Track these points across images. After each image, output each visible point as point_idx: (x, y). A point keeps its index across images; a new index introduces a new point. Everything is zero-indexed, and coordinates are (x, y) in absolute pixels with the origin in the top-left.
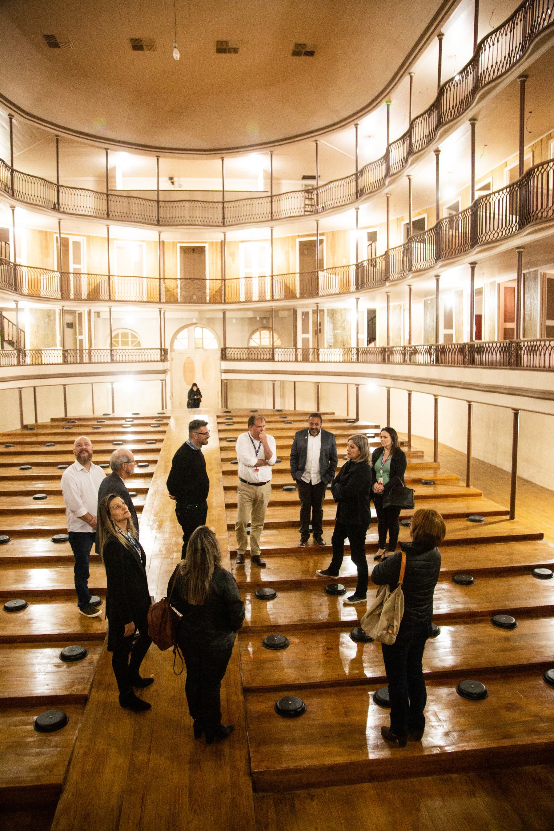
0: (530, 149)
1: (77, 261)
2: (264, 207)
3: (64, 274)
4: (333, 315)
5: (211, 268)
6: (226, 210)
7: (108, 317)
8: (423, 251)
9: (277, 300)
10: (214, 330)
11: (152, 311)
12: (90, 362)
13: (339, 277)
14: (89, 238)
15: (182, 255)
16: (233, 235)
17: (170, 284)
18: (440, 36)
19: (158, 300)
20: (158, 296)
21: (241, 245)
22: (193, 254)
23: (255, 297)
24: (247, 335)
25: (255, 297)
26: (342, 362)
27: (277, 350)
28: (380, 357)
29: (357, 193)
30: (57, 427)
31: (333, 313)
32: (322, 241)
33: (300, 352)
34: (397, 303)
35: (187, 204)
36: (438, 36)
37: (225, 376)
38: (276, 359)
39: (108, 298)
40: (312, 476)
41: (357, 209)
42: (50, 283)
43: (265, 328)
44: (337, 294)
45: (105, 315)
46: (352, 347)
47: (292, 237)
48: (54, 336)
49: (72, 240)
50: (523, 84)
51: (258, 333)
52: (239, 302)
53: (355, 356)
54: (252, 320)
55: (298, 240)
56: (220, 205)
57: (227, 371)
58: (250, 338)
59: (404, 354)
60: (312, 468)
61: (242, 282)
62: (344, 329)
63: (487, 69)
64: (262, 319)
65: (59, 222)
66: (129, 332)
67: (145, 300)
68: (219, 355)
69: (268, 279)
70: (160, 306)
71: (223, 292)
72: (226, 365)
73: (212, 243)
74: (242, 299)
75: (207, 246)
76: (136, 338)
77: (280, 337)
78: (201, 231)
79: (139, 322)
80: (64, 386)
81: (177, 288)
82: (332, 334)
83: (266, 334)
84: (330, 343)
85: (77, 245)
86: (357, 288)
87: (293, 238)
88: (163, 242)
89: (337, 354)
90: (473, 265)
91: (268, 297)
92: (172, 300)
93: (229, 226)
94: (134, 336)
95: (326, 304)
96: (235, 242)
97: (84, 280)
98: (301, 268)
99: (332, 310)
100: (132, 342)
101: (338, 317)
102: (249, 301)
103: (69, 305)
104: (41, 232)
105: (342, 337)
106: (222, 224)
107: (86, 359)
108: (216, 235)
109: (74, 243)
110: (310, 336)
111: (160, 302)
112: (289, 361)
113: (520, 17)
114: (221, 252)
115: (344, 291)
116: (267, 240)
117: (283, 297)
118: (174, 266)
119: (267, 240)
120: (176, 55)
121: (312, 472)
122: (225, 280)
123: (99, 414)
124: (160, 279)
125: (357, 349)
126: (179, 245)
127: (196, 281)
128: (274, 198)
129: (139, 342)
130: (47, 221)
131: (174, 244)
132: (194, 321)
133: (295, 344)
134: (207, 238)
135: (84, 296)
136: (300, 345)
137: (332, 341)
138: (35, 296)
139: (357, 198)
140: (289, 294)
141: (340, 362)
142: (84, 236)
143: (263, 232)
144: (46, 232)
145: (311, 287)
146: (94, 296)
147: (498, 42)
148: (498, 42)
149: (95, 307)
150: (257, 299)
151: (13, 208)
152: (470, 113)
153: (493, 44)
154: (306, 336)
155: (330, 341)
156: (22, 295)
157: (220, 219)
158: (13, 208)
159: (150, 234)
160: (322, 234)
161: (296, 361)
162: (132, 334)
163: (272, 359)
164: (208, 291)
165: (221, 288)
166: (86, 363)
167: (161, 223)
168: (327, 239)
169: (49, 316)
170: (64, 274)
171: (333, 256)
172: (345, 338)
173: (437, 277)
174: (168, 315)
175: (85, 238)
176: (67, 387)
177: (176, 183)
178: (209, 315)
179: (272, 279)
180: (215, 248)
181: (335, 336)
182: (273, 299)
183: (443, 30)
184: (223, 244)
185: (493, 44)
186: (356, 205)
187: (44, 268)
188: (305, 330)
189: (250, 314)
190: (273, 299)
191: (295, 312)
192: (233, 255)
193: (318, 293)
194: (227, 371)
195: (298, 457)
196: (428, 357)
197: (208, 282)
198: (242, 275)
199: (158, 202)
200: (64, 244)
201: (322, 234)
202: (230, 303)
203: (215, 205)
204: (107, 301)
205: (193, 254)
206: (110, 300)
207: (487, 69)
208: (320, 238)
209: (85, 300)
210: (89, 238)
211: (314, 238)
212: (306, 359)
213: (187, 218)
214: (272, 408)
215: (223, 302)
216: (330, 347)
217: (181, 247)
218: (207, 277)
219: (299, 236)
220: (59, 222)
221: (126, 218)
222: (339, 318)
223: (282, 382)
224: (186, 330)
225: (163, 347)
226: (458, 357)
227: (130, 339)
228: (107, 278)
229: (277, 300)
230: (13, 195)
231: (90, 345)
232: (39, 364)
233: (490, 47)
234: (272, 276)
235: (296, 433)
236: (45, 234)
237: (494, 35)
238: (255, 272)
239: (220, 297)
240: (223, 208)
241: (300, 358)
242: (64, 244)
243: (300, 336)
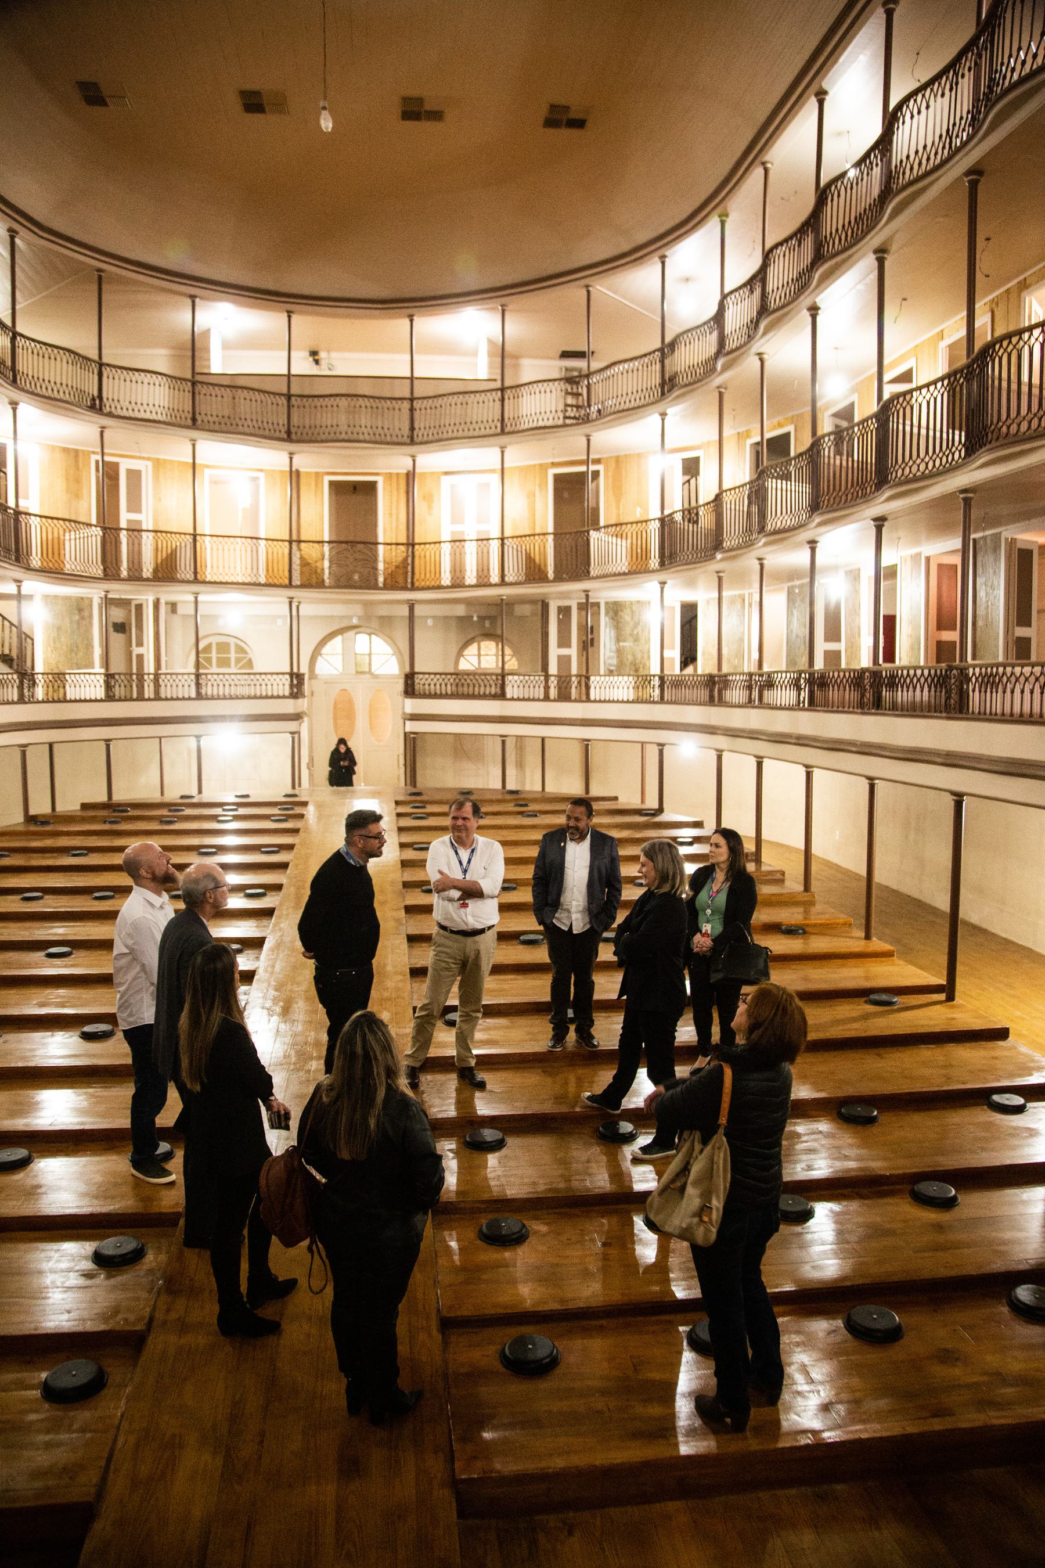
0: (987, 308)
1: (135, 505)
2: (487, 410)
3: (110, 531)
4: (616, 613)
5: (388, 524)
6: (417, 414)
7: (193, 612)
8: (787, 495)
9: (511, 584)
10: (392, 641)
11: (275, 604)
12: (157, 698)
13: (629, 541)
14: (158, 464)
15: (334, 496)
16: (429, 460)
17: (310, 551)
18: (821, 96)
19: (287, 582)
20: (287, 574)
21: (444, 479)
22: (354, 496)
23: (471, 578)
24: (454, 649)
25: (471, 578)
26: (633, 702)
27: (510, 677)
28: (704, 694)
29: (662, 385)
30: (93, 819)
31: (616, 609)
32: (596, 474)
33: (553, 682)
34: (737, 592)
35: (343, 402)
36: (816, 95)
37: (411, 726)
38: (509, 696)
39: (191, 577)
40: (574, 916)
41: (663, 415)
42: (82, 548)
43: (489, 636)
44: (624, 574)
45: (186, 609)
46: (652, 673)
47: (541, 465)
48: (89, 646)
49: (125, 465)
50: (974, 186)
51: (475, 645)
52: (440, 587)
53: (657, 692)
54: (463, 621)
55: (552, 472)
56: (406, 405)
57: (415, 717)
58: (460, 654)
59: (750, 688)
60: (574, 903)
61: (446, 549)
62: (636, 640)
63: (908, 157)
64: (482, 619)
65: (102, 433)
66: (232, 641)
67: (262, 580)
68: (400, 686)
69: (495, 545)
70: (291, 593)
71: (409, 568)
72: (412, 705)
73: (389, 476)
74: (446, 580)
75: (380, 480)
76: (246, 652)
77: (516, 653)
78: (372, 452)
79: (249, 622)
80: (108, 742)
81: (324, 559)
82: (614, 648)
83: (489, 647)
84: (611, 665)
85: (134, 476)
86: (662, 564)
87: (543, 468)
88: (298, 472)
89: (623, 687)
90: (880, 522)
91: (495, 578)
92: (312, 581)
93: (421, 443)
94: (240, 650)
95: (605, 593)
96: (433, 473)
97: (148, 542)
98: (555, 528)
99: (616, 603)
100: (238, 660)
101: (626, 616)
102: (458, 584)
103: (118, 590)
104: (65, 450)
105: (634, 655)
106: (408, 441)
107: (149, 691)
108: (398, 461)
109: (129, 472)
110: (573, 652)
111: (290, 585)
112: (534, 700)
113: (968, 62)
114: (407, 493)
115: (638, 569)
116: (493, 471)
117: (522, 578)
118: (318, 517)
119: (493, 471)
120: (327, 123)
121: (573, 910)
122: (413, 545)
123: (172, 795)
124: (290, 542)
125: (662, 678)
126: (327, 479)
127: (360, 546)
128: (508, 393)
129: (250, 661)
130: (77, 430)
131: (318, 476)
132: (355, 621)
133: (545, 668)
134: (383, 465)
135: (147, 571)
136: (553, 669)
137: (615, 662)
138: (54, 572)
139: (663, 394)
140: (534, 573)
141: (628, 702)
142: (149, 459)
143: (486, 456)
144: (76, 451)
145: (574, 561)
146: (166, 572)
147: (928, 107)
148: (928, 107)
149: (169, 593)
150: (474, 581)
151: (14, 405)
152: (875, 239)
153: (919, 112)
154: (564, 651)
155: (611, 661)
156: (28, 568)
157: (406, 431)
158: (14, 405)
159: (273, 457)
160: (598, 461)
161: (547, 698)
162: (237, 645)
163: (501, 696)
164: (381, 566)
165: (406, 559)
166: (149, 699)
167: (293, 437)
168: (606, 470)
169: (80, 610)
170: (110, 531)
171: (618, 501)
172: (639, 656)
173: (813, 544)
174: (306, 610)
175: (150, 464)
176: (112, 744)
177: (323, 363)
178: (383, 611)
179: (503, 545)
180: (394, 484)
181: (619, 652)
182: (503, 583)
183: (825, 85)
184: (410, 477)
185: (919, 112)
186: (660, 407)
187: (73, 518)
188: (564, 641)
189: (460, 610)
190: (503, 583)
191: (545, 606)
192: (429, 498)
193: (589, 572)
194: (415, 717)
195: (548, 879)
196: (794, 693)
197: (381, 549)
198: (446, 536)
199: (289, 397)
200: (109, 474)
201: (598, 461)
202: (423, 589)
203: (397, 405)
204: (188, 582)
205: (354, 496)
206: (196, 581)
207: (908, 157)
208: (593, 468)
209: (148, 580)
210: (158, 464)
211: (583, 469)
212: (564, 696)
213: (344, 428)
214: (500, 787)
215: (409, 586)
216: (611, 673)
217: (332, 483)
218: (381, 540)
219: (554, 465)
220: (102, 433)
221: (228, 427)
222: (628, 618)
223: (519, 738)
224: (339, 638)
225: (295, 670)
226: (851, 695)
227: (233, 655)
228: (190, 539)
229: (511, 584)
230: (15, 381)
231: (158, 665)
232: (59, 701)
233: (912, 117)
234: (502, 539)
235: (544, 836)
236: (74, 456)
237: (920, 96)
238: (471, 532)
239: (403, 577)
240: (412, 410)
241: (553, 693)
242: (109, 474)
243: (554, 651)
